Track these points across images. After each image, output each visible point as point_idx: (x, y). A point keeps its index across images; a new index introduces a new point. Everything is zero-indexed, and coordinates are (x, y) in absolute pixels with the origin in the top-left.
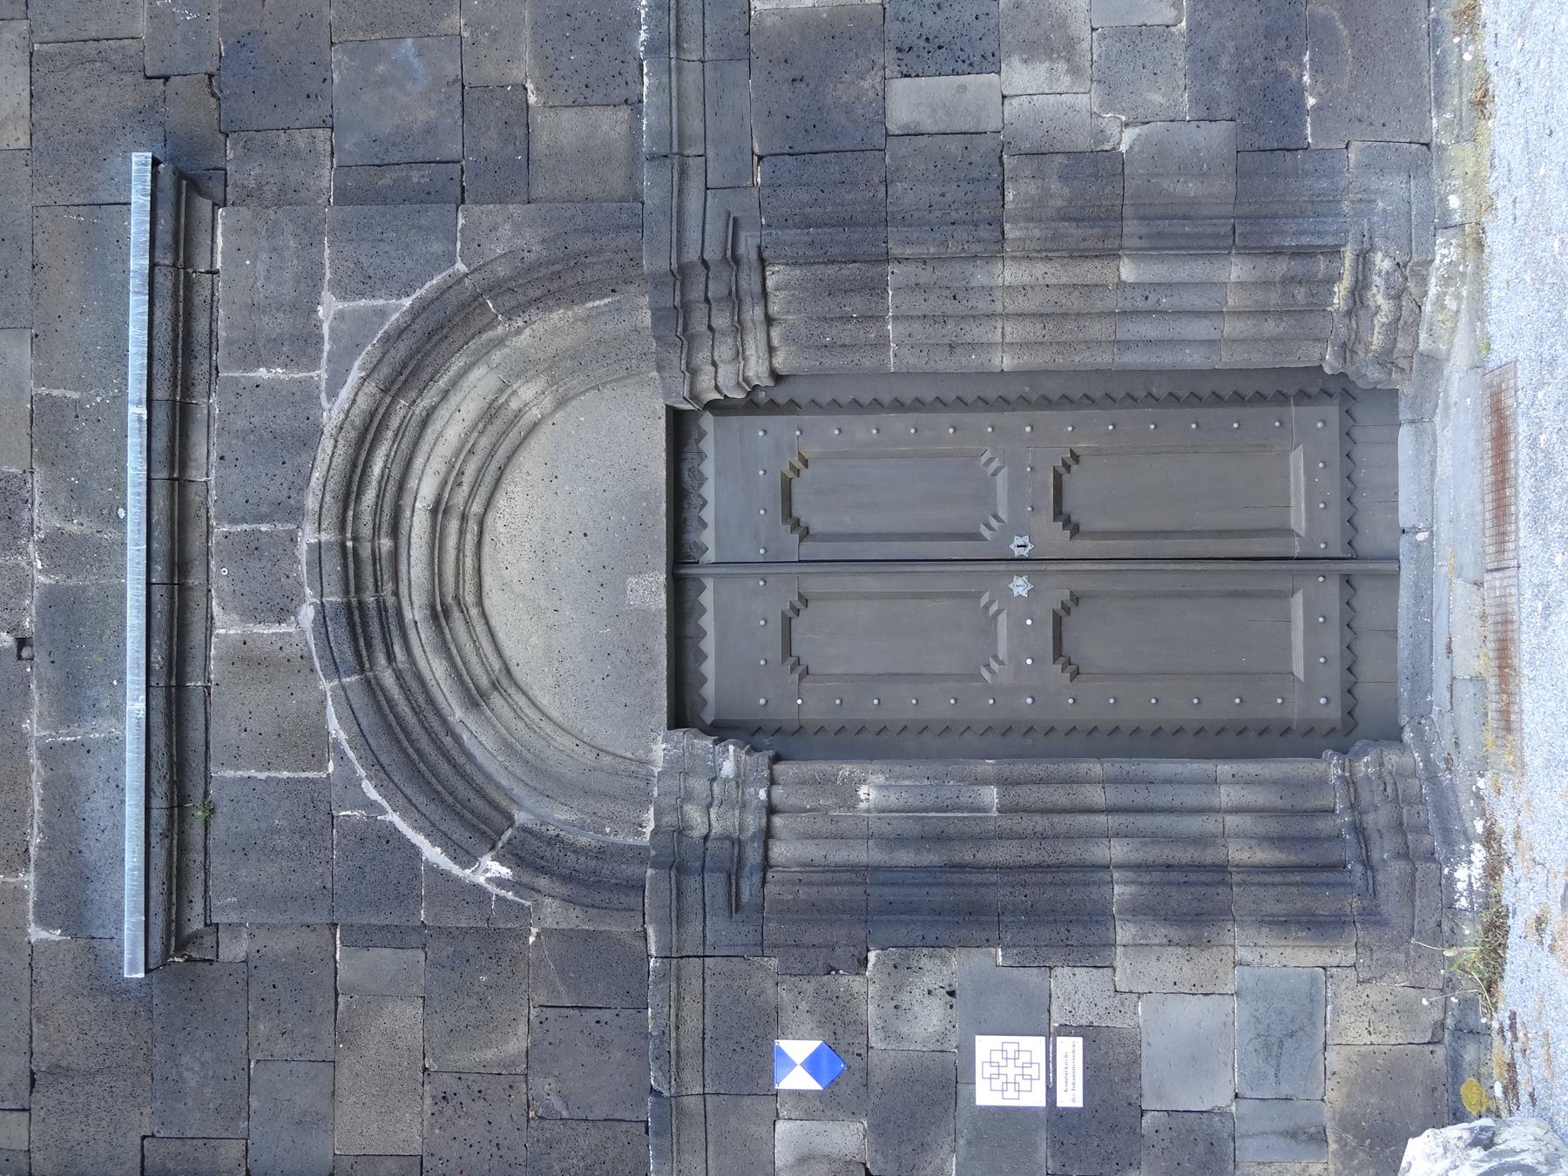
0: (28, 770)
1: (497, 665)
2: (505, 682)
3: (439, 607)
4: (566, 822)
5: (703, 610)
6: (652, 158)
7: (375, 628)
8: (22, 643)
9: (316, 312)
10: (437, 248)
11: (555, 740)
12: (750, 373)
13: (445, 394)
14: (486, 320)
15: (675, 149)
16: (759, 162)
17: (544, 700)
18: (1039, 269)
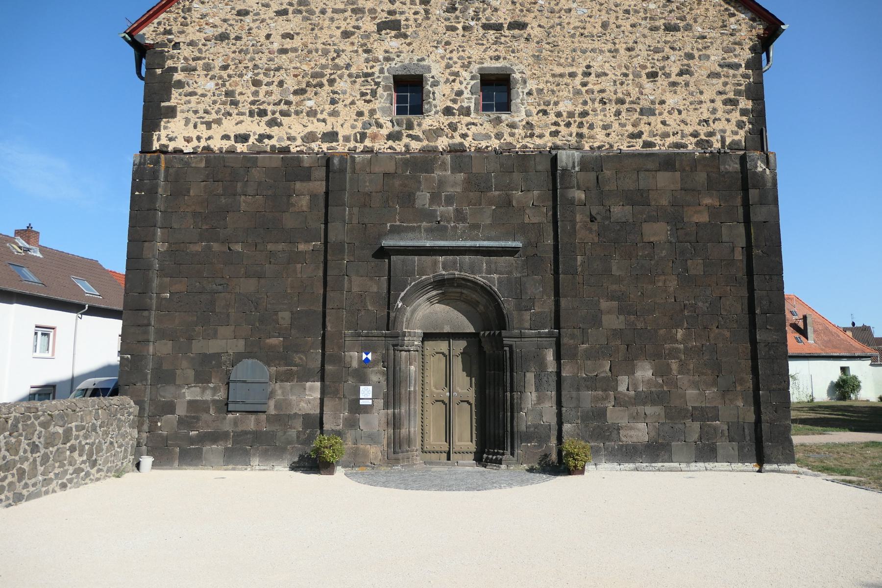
8: (439, 222)
10: (506, 295)
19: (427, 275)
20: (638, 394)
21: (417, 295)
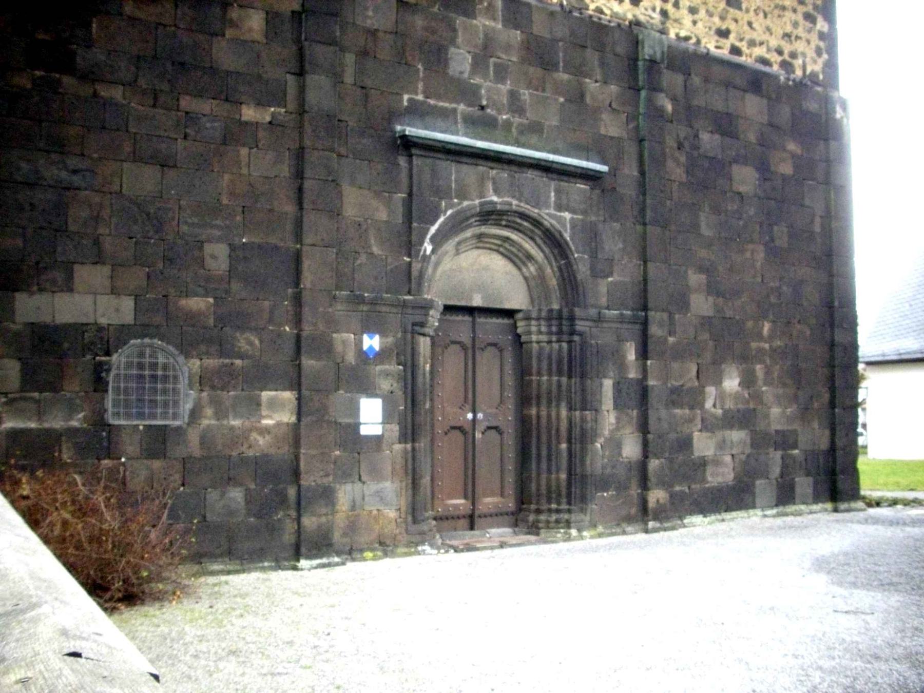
0: (451, 103)
6: (600, 313)
20: (726, 412)
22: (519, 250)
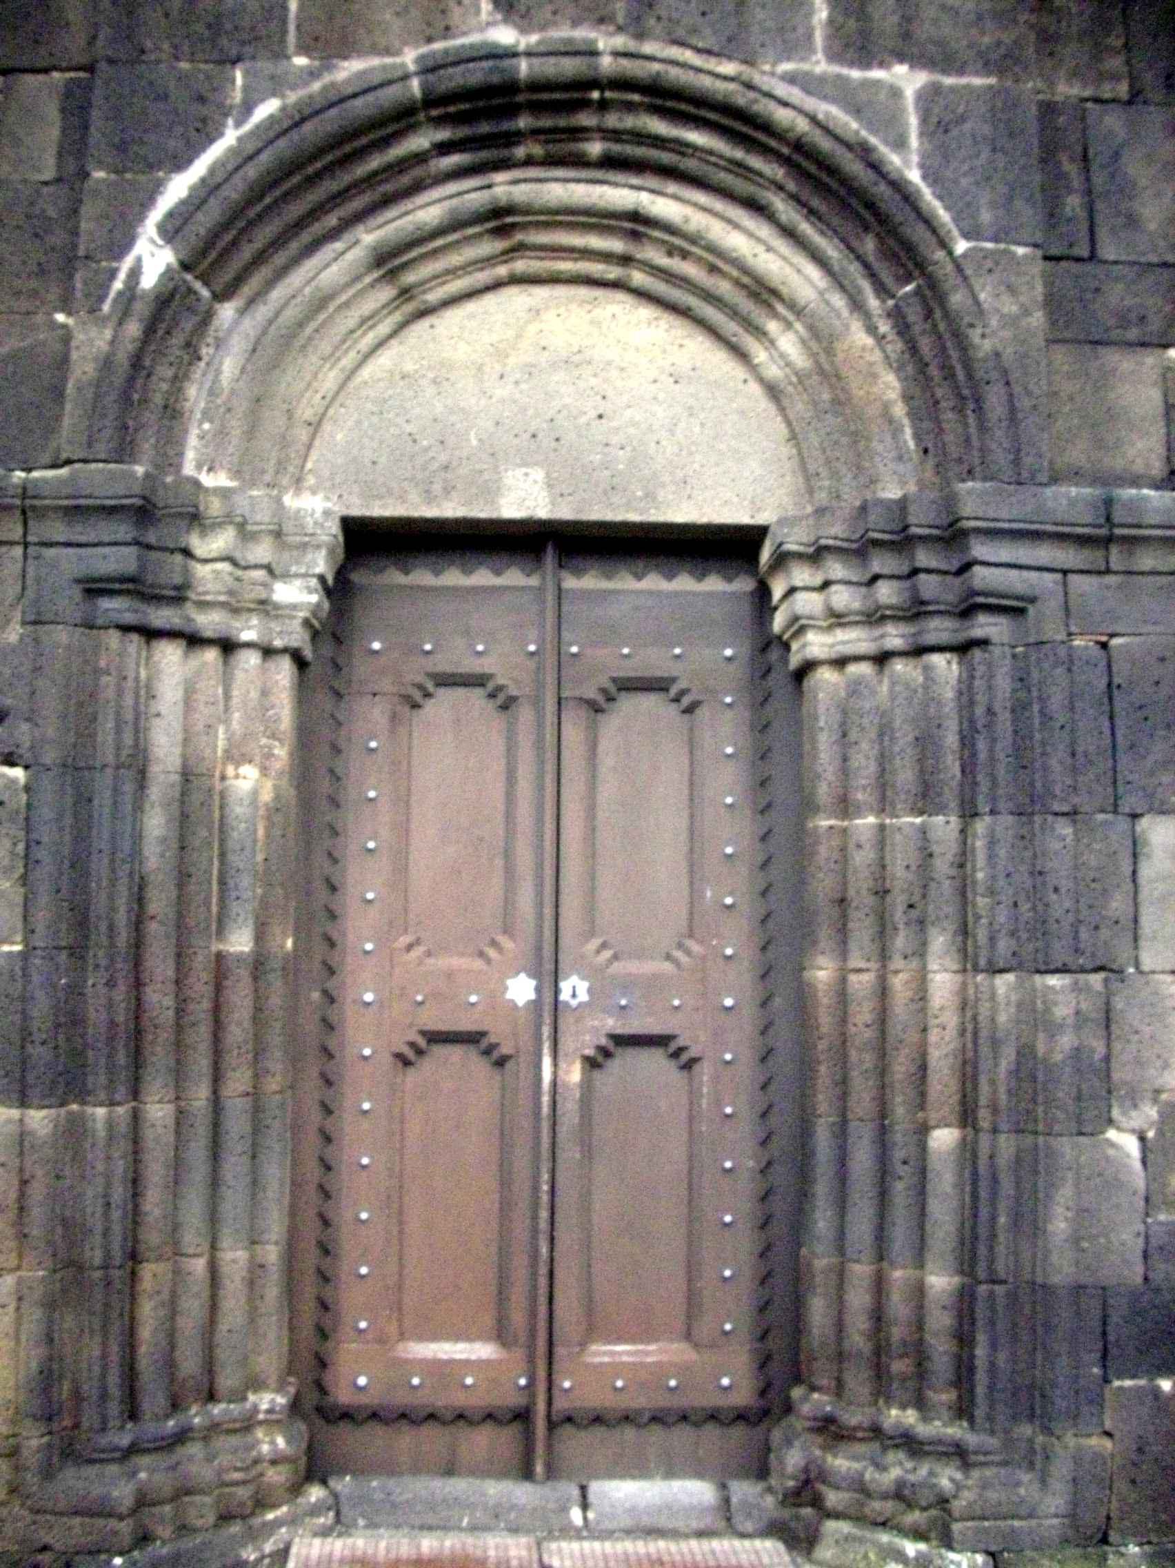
1: (433, 297)
2: (409, 308)
3: (509, 220)
4: (218, 372)
5: (498, 573)
6: (1109, 502)
7: (485, 128)
9: (901, 61)
11: (331, 369)
12: (811, 636)
13: (789, 233)
14: (888, 280)
15: (1118, 531)
16: (1097, 642)
17: (384, 360)
18: (951, 1020)
19: (375, 50)
21: (295, 210)
22: (713, 269)
